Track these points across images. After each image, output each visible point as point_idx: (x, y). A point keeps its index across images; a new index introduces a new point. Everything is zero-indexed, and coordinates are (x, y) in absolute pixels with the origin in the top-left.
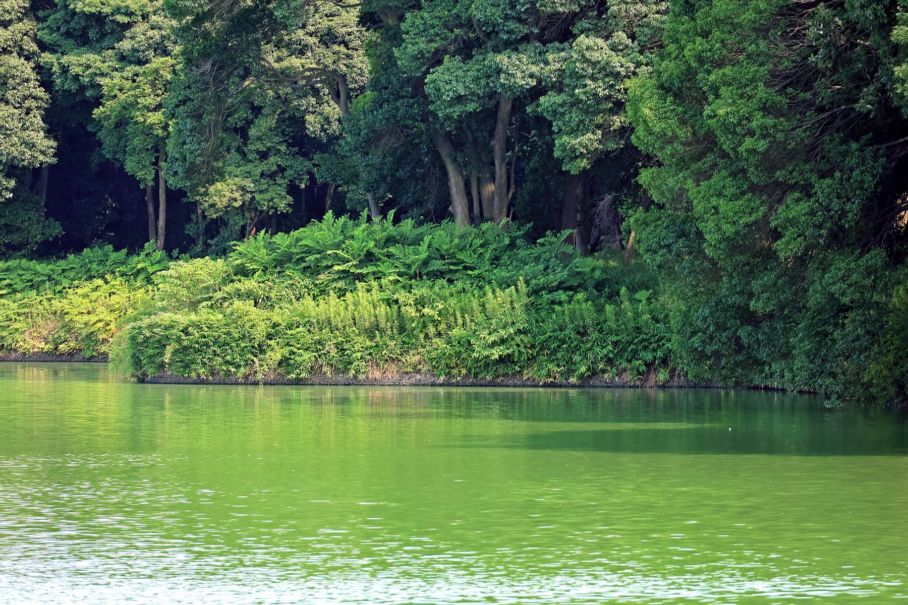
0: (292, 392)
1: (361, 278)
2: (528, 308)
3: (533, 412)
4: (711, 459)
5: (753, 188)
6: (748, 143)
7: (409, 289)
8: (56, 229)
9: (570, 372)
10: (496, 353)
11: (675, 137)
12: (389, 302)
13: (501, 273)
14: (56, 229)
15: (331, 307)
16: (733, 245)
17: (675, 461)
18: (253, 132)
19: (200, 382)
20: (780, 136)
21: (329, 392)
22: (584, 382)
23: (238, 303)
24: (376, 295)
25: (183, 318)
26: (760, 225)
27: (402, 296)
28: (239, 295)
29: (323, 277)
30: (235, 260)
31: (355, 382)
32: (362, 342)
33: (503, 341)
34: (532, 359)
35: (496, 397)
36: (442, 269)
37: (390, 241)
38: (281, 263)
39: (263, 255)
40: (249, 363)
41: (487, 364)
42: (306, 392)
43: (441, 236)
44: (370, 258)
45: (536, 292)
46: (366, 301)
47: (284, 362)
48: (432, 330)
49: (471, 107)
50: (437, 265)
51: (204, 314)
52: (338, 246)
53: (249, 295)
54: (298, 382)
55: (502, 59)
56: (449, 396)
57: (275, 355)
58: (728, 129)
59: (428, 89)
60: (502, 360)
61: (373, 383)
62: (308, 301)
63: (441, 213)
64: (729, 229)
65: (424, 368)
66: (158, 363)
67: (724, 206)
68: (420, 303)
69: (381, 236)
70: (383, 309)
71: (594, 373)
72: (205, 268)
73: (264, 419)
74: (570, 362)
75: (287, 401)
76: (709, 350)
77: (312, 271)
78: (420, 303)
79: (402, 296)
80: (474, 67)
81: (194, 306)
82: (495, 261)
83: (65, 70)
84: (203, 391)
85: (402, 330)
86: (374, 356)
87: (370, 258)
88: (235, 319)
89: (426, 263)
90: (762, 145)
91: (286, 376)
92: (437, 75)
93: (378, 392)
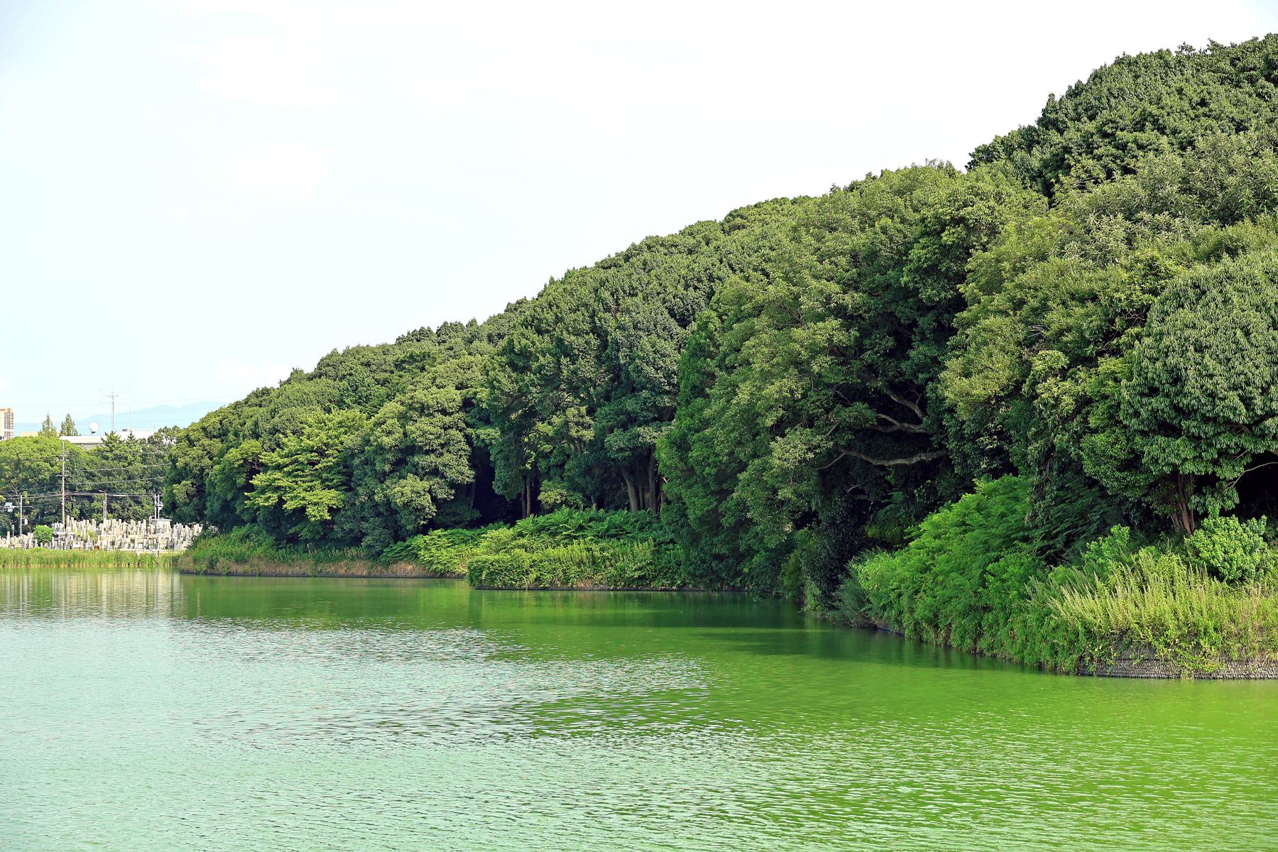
0: (542, 594)
1: (576, 538)
2: (653, 553)
3: (657, 604)
4: (666, 632)
5: (713, 493)
6: (707, 470)
7: (597, 543)
8: (477, 514)
9: (672, 584)
10: (636, 575)
11: (676, 468)
12: (588, 550)
13: (641, 535)
14: (477, 514)
15: (561, 551)
16: (701, 520)
17: (684, 631)
18: (566, 467)
19: (499, 589)
20: (723, 467)
21: (559, 594)
22: (680, 589)
23: (517, 550)
24: (582, 546)
25: (491, 558)
26: (715, 510)
27: (594, 546)
28: (519, 547)
29: (558, 537)
30: (517, 529)
31: (572, 589)
32: (575, 569)
33: (640, 569)
34: (654, 578)
35: (638, 597)
36: (615, 533)
37: (591, 520)
38: (540, 530)
39: (531, 527)
40: (521, 580)
41: (633, 580)
42: (547, 594)
43: (618, 517)
44: (581, 528)
45: (659, 544)
46: (577, 549)
47: (538, 579)
48: (608, 563)
49: (626, 454)
50: (613, 531)
51: (502, 556)
52: (566, 522)
53: (523, 546)
54: (545, 589)
55: (641, 430)
56: (615, 596)
57: (533, 576)
58: (698, 463)
59: (606, 445)
60: (640, 578)
61: (580, 589)
62: (550, 549)
63: (622, 505)
64: (699, 513)
65: (605, 582)
66: (483, 579)
67: (698, 502)
68: (602, 550)
69: (587, 517)
70: (585, 553)
71: (684, 584)
72: (504, 533)
73: (529, 606)
74: (673, 579)
75: (538, 598)
76: (697, 573)
77: (553, 534)
78: (602, 550)
79: (594, 546)
80: (628, 435)
81: (497, 551)
82: (641, 529)
83: (478, 437)
84: (500, 593)
85: (594, 563)
86: (580, 576)
87: (581, 528)
88: (514, 559)
89: (607, 530)
90: (714, 471)
91: (537, 586)
92: (610, 438)
93: (581, 594)
